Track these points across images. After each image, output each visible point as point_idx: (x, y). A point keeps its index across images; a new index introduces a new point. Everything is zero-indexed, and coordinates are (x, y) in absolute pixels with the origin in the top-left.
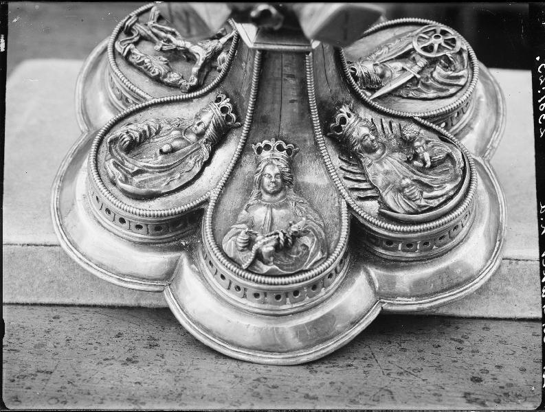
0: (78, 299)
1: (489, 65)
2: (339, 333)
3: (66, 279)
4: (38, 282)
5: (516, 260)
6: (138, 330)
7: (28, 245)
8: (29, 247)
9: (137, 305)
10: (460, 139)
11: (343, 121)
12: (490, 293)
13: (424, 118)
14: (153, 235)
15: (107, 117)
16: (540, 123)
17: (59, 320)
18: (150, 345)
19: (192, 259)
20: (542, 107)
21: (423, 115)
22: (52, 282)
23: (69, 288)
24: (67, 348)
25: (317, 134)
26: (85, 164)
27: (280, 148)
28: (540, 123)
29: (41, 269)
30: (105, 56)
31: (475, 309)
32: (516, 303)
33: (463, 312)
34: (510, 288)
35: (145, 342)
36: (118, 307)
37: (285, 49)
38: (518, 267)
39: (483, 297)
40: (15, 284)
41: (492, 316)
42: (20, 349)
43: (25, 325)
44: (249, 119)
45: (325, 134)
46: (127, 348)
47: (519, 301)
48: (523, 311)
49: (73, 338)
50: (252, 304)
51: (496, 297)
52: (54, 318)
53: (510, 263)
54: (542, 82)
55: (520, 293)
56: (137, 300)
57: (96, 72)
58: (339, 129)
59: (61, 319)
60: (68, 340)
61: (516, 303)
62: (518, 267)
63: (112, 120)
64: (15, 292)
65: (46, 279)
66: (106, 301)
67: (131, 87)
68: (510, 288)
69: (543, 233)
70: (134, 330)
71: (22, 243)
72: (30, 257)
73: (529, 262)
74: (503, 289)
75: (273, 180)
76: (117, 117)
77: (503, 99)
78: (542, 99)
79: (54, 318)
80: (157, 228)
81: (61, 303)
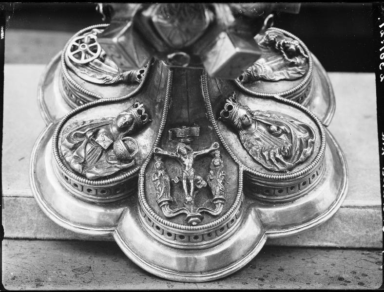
1: (331, 66)
2: (236, 261)
9: (34, 237)
11: (230, 108)
13: (284, 96)
14: (100, 196)
15: (63, 111)
16: (380, 68)
19: (135, 214)
20: (382, 56)
21: (282, 94)
28: (380, 68)
30: (60, 63)
33: (300, 243)
45: (216, 119)
50: (174, 243)
54: (382, 34)
56: (35, 234)
58: (226, 114)
63: (69, 114)
67: (76, 85)
69: (383, 154)
76: (70, 113)
77: (334, 98)
78: (382, 48)
80: (103, 192)
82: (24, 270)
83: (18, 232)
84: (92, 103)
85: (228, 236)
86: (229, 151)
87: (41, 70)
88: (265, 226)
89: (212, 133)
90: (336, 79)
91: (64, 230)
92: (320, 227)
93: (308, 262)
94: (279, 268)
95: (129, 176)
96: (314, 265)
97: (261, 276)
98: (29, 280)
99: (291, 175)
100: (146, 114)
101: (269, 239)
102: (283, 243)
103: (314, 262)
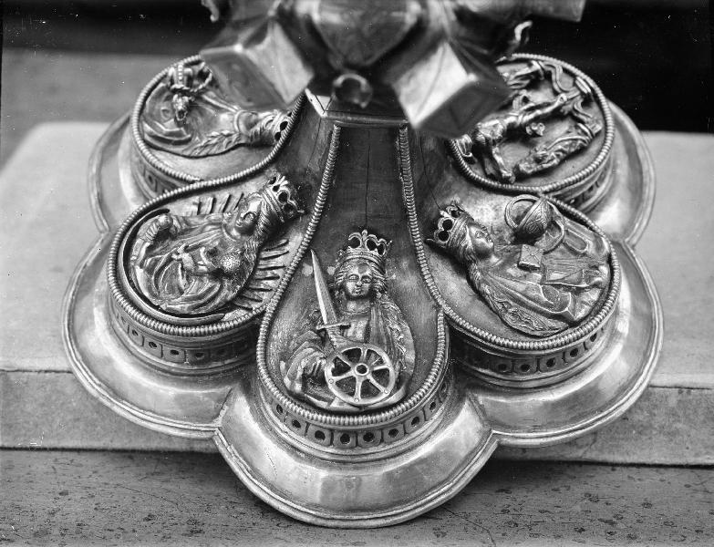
0: (111, 441)
1: (648, 120)
3: (95, 416)
4: (58, 421)
5: (688, 388)
6: (185, 491)
7: (46, 371)
8: (47, 374)
9: (189, 449)
10: (593, 219)
12: (654, 432)
15: (133, 205)
17: (67, 497)
18: (192, 532)
22: (78, 419)
23: (99, 428)
24: (79, 536)
25: (421, 247)
26: (103, 272)
27: (371, 245)
29: (63, 404)
30: (127, 130)
31: (634, 454)
32: (688, 445)
34: (679, 425)
35: (185, 527)
36: (165, 452)
37: (553, 442)
38: (691, 397)
39: (644, 438)
40: (28, 423)
41: (657, 462)
42: (14, 537)
43: (21, 504)
44: (318, 213)
46: (160, 535)
47: (692, 443)
48: (697, 455)
49: (86, 522)
51: (662, 437)
52: (60, 494)
53: (680, 392)
55: (693, 432)
57: (116, 150)
59: (70, 496)
60: (79, 525)
61: (688, 445)
62: (691, 397)
64: (28, 433)
65: (70, 417)
66: (148, 444)
68: (679, 425)
70: (169, 510)
71: (37, 369)
72: (48, 388)
73: (706, 391)
74: (670, 426)
75: (359, 283)
79: (60, 494)
81: (89, 447)
82: (166, 503)
83: (158, 439)
84: (180, 190)
85: (418, 440)
86: (303, 250)
87: (94, 132)
88: (491, 422)
89: (402, 248)
90: (660, 147)
91: (143, 431)
92: (610, 427)
93: (696, 491)
94: (643, 501)
95: (231, 328)
96: (708, 496)
97: (610, 517)
98: (176, 521)
99: (575, 335)
100: (381, 240)
101: (501, 447)
102: (554, 455)
103: (708, 492)
